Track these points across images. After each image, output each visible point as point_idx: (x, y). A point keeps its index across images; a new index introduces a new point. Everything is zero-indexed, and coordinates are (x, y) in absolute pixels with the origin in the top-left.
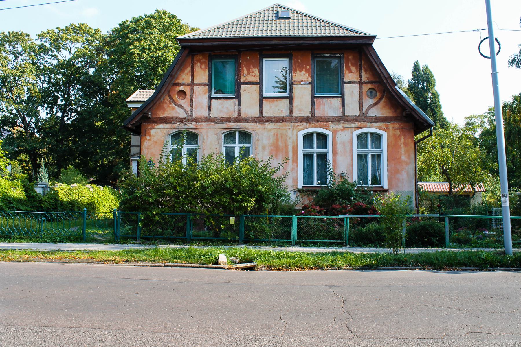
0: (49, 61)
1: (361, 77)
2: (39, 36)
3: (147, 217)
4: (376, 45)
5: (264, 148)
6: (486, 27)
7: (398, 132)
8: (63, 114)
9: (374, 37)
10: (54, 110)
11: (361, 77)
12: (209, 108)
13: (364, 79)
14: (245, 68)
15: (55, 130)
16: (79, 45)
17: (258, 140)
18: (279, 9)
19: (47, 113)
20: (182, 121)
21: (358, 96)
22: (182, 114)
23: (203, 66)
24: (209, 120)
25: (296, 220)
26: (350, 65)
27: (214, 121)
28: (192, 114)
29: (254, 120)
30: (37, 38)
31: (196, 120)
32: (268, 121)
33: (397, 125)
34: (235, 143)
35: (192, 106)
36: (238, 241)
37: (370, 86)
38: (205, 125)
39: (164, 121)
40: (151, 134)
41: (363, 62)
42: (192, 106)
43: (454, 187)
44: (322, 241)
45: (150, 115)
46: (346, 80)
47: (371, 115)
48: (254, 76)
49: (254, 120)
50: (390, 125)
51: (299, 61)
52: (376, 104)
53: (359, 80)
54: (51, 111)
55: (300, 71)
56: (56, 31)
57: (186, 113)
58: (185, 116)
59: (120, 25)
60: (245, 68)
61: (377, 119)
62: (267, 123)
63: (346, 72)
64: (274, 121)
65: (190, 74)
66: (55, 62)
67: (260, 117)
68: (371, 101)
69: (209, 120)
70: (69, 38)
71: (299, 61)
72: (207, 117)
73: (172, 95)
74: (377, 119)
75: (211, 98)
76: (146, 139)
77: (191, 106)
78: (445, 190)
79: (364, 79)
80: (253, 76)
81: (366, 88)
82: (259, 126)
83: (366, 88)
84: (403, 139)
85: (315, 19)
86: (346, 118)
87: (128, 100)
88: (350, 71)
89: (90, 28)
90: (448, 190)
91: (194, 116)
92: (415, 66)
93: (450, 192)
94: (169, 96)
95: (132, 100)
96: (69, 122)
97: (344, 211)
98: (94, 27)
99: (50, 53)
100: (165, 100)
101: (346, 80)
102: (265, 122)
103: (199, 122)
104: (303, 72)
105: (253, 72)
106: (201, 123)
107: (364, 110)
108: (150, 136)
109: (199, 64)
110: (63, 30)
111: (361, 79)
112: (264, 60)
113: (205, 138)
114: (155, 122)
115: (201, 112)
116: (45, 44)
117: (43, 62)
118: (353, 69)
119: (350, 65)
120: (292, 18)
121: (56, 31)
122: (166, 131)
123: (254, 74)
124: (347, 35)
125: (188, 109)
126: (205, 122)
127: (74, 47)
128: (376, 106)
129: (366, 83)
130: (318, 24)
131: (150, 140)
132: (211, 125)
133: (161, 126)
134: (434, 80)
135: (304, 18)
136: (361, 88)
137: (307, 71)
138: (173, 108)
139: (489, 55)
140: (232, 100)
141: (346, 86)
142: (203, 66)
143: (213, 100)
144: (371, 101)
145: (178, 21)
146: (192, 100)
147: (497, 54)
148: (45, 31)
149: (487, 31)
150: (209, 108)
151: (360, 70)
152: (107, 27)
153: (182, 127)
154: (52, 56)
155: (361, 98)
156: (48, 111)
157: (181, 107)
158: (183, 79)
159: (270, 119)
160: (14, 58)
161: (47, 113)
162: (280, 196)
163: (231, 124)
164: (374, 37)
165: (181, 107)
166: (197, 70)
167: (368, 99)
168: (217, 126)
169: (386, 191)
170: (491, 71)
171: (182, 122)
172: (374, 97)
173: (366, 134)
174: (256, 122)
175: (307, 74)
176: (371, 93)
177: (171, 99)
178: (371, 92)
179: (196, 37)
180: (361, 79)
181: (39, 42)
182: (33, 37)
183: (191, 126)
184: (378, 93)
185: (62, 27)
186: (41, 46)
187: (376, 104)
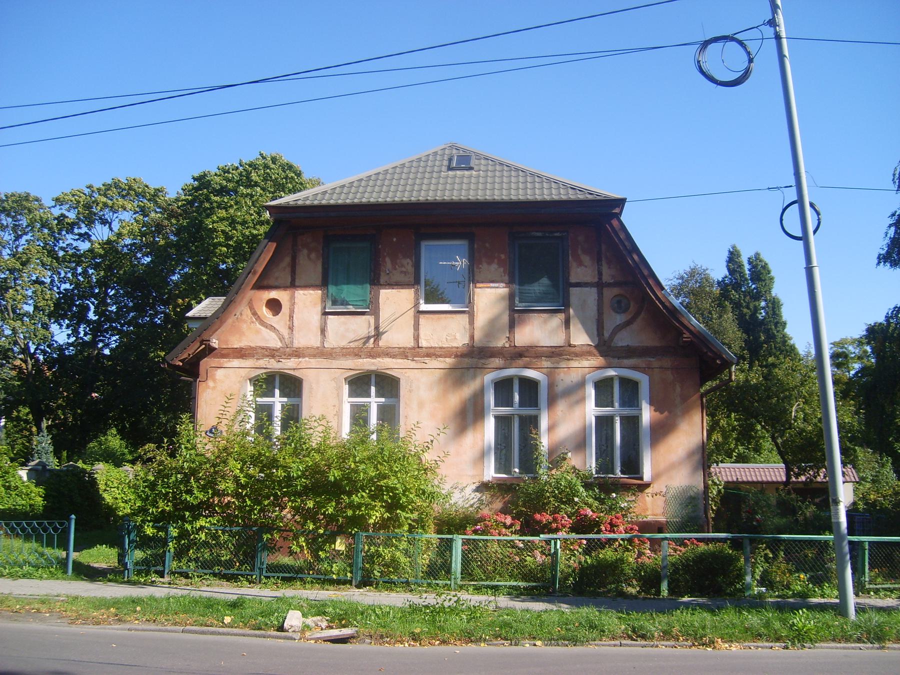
0: (75, 244)
1: (600, 274)
2: (57, 200)
3: (184, 534)
4: (629, 218)
5: (421, 405)
6: (793, 183)
7: (669, 376)
8: (95, 337)
9: (621, 202)
10: (81, 330)
11: (600, 274)
12: (323, 331)
13: (606, 278)
14: (388, 260)
15: (73, 367)
16: (126, 216)
17: (410, 391)
18: (454, 151)
19: (69, 335)
20: (272, 353)
21: (595, 308)
22: (274, 342)
23: (313, 256)
24: (322, 353)
25: (460, 542)
26: (580, 252)
27: (331, 354)
28: (292, 342)
29: (404, 353)
30: (53, 203)
31: (297, 353)
32: (428, 355)
33: (667, 362)
34: (369, 396)
35: (291, 328)
36: (350, 582)
37: (616, 291)
38: (313, 362)
39: (241, 353)
40: (217, 377)
41: (604, 247)
42: (291, 328)
43: (797, 475)
44: (508, 584)
45: (215, 343)
46: (573, 279)
47: (620, 344)
48: (405, 273)
49: (404, 353)
50: (655, 362)
51: (487, 245)
52: (628, 323)
53: (596, 280)
54: (76, 332)
55: (489, 263)
56: (87, 191)
57: (282, 339)
58: (279, 345)
59: (195, 179)
60: (388, 260)
61: (629, 352)
62: (427, 360)
63: (573, 265)
64: (440, 356)
65: (288, 270)
66: (84, 246)
67: (414, 348)
68: (619, 319)
69: (322, 353)
70: (110, 203)
71: (487, 245)
72: (318, 348)
73: (255, 307)
74: (629, 352)
75: (325, 314)
76: (208, 387)
77: (290, 328)
78: (779, 479)
79: (606, 278)
80: (401, 272)
81: (609, 293)
82: (412, 364)
83: (609, 293)
84: (678, 389)
85: (517, 170)
86: (573, 349)
87: (190, 314)
88: (580, 264)
89: (147, 186)
90: (784, 479)
91: (296, 344)
92: (731, 253)
93: (787, 482)
94: (252, 308)
95: (197, 315)
96: (107, 352)
97: (554, 525)
98: (153, 185)
99: (76, 231)
100: (244, 317)
101: (573, 279)
102: (424, 356)
103: (304, 357)
104: (494, 266)
105: (402, 266)
106: (307, 359)
107: (606, 335)
108: (214, 381)
109: (305, 251)
110: (99, 190)
111: (600, 279)
112: (424, 245)
113: (314, 386)
114: (224, 356)
115: (307, 338)
116: (67, 214)
117: (64, 245)
118: (586, 259)
119: (580, 252)
120: (476, 168)
121: (87, 191)
122: (243, 372)
123: (404, 269)
124: (573, 197)
125: (285, 332)
126: (314, 356)
127: (117, 220)
128: (628, 328)
129: (609, 285)
130: (521, 179)
131: (214, 388)
132: (324, 363)
133: (236, 363)
134: (772, 279)
135: (498, 168)
136: (600, 294)
137: (501, 263)
138: (258, 332)
139: (799, 234)
140: (364, 317)
141: (573, 290)
142: (313, 256)
143: (330, 317)
144: (619, 319)
145: (299, 175)
146: (291, 317)
147: (815, 232)
148: (68, 191)
149: (794, 189)
150: (323, 331)
151: (599, 261)
152: (174, 184)
153: (273, 365)
154: (80, 235)
155: (600, 313)
156: (70, 332)
157: (272, 328)
158: (277, 278)
159: (432, 351)
160: (13, 238)
161: (69, 335)
162: (432, 496)
163: (361, 360)
164: (621, 202)
165: (272, 328)
166: (301, 262)
167: (613, 314)
168: (336, 363)
169: (647, 485)
170: (803, 264)
171: (273, 356)
172: (624, 312)
173: (610, 380)
174: (406, 357)
175: (502, 269)
176: (619, 306)
177: (255, 314)
178: (619, 302)
179: (300, 203)
180: (600, 279)
181: (56, 212)
182: (48, 202)
183: (288, 365)
184: (632, 304)
185: (97, 184)
186: (61, 219)
187: (628, 323)
